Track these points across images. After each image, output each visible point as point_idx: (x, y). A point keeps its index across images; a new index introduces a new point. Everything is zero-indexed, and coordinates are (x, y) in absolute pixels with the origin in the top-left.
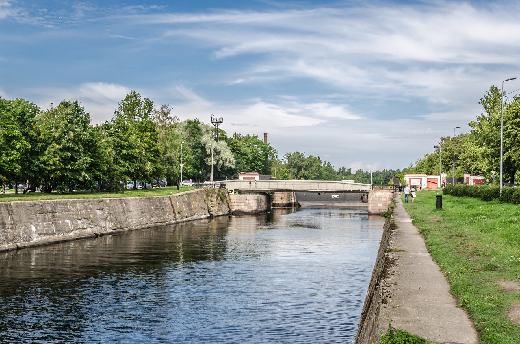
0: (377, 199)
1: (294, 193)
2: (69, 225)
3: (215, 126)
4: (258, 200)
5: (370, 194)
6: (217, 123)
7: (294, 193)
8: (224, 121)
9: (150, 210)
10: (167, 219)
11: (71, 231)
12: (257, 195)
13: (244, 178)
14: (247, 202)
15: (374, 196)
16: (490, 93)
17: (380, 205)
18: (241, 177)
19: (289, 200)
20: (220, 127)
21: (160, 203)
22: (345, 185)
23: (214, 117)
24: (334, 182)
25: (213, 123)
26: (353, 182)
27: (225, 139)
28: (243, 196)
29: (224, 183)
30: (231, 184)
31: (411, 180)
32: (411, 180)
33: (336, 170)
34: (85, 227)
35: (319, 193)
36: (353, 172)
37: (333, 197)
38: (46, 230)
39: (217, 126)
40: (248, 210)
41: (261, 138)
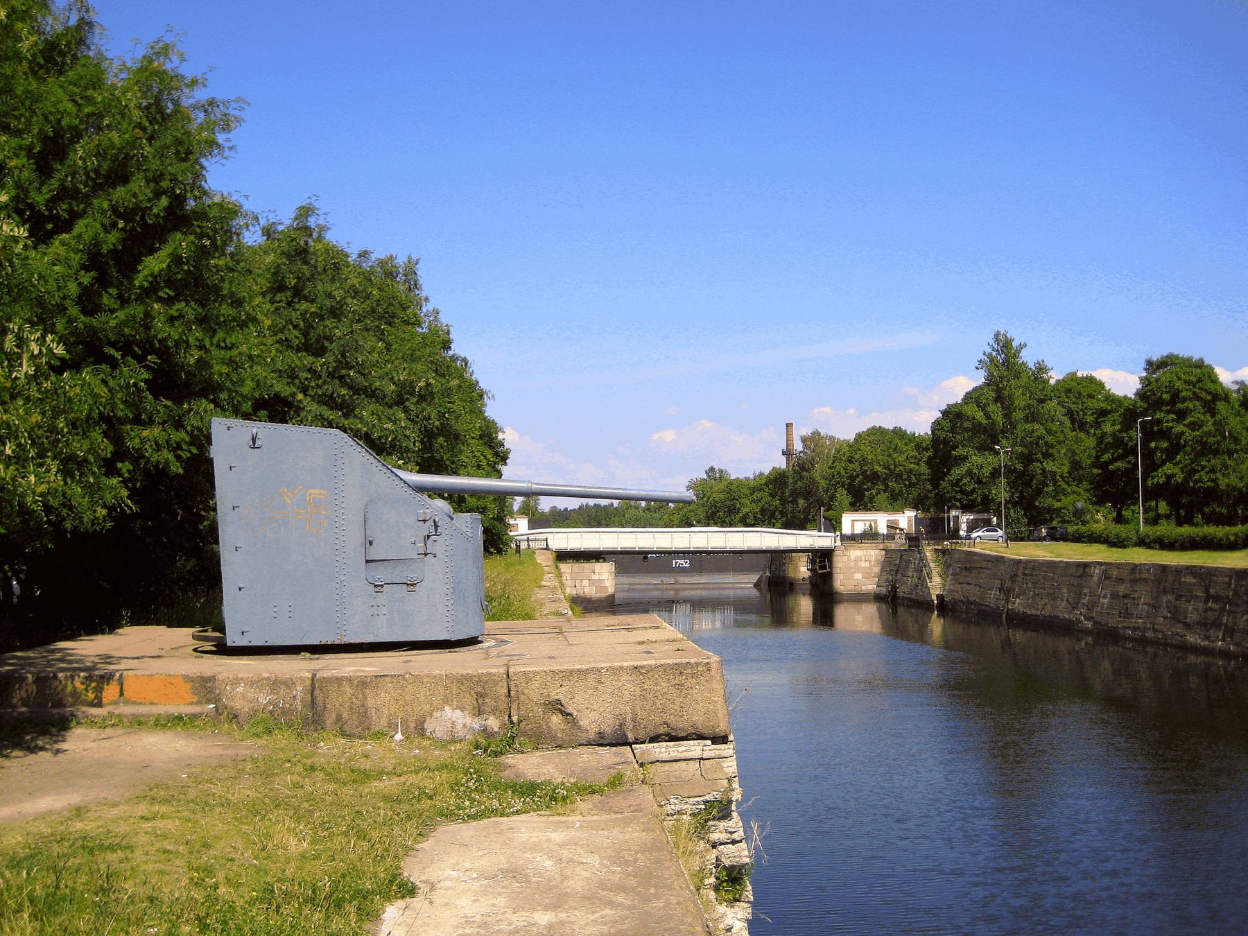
0: (852, 564)
14: (596, 577)
16: (996, 346)
17: (858, 576)
28: (586, 566)
31: (855, 523)
32: (855, 523)
37: (676, 563)
40: (598, 595)
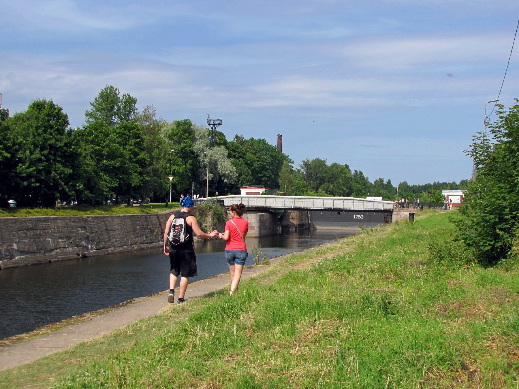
1: (309, 211)
2: (50, 244)
3: (212, 128)
4: (260, 219)
5: (394, 213)
6: (215, 125)
7: (309, 211)
8: (222, 123)
9: (135, 230)
10: (154, 240)
11: (52, 250)
12: (259, 214)
13: (247, 193)
15: (398, 216)
18: (243, 192)
19: (302, 220)
20: (219, 129)
21: (147, 221)
22: (365, 203)
23: (211, 118)
24: (236, 197)
25: (209, 125)
26: (379, 199)
27: (225, 144)
29: (222, 199)
30: (229, 200)
31: (449, 197)
32: (449, 197)
33: (372, 181)
34: (67, 246)
35: (339, 211)
36: (458, 183)
37: (356, 217)
38: (27, 248)
39: (215, 129)
41: (273, 142)
